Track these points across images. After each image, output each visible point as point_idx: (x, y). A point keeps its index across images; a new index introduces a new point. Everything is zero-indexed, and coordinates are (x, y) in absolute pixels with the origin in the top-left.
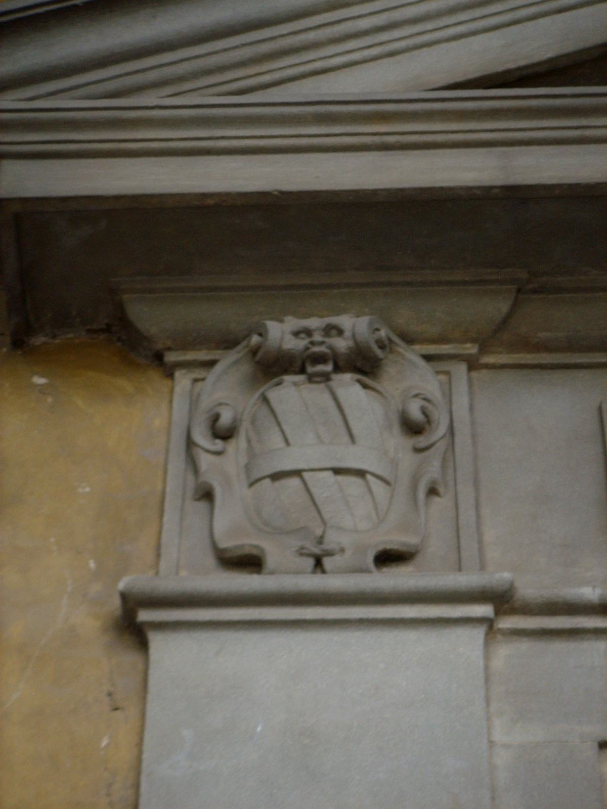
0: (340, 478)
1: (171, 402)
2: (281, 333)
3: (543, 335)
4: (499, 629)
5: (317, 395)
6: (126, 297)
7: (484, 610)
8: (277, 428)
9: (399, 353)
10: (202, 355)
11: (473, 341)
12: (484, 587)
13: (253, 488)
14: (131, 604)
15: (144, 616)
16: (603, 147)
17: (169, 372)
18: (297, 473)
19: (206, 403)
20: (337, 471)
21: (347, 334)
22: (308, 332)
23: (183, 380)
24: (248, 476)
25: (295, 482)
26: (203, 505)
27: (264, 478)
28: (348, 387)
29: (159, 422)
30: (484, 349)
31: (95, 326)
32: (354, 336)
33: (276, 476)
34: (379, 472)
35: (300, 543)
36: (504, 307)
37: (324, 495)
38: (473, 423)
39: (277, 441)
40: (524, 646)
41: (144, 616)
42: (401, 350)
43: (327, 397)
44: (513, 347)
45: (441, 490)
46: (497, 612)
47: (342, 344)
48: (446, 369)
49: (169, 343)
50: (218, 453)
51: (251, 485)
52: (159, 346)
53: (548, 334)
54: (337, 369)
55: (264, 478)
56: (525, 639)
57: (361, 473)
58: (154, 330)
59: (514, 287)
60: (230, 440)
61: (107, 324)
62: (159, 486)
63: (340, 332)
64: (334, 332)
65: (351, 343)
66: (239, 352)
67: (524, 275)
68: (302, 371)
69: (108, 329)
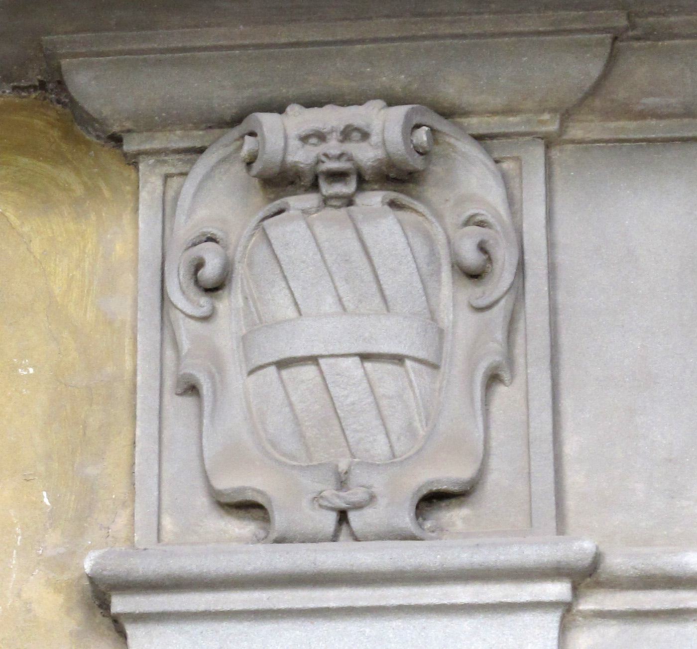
0: (368, 365)
1: (136, 210)
2: (283, 135)
3: (650, 101)
4: (580, 611)
5: (332, 228)
6: (64, 62)
7: (559, 590)
8: (283, 284)
9: (449, 144)
10: (177, 139)
11: (553, 111)
12: (559, 562)
13: (253, 377)
14: (99, 594)
15: (120, 604)
16: (693, 150)
17: (133, 160)
18: (314, 359)
19: (185, 227)
20: (365, 357)
21: (375, 139)
22: (321, 137)
23: (151, 183)
24: (247, 359)
25: (309, 371)
26: (188, 402)
27: (269, 364)
28: (380, 223)
29: (120, 249)
30: (567, 115)
31: (23, 83)
32: (384, 143)
33: (282, 364)
34: (421, 355)
35: (319, 487)
36: (595, 69)
37: (349, 401)
38: (551, 245)
39: (283, 308)
40: (612, 631)
41: (120, 604)
42: (452, 141)
43: (350, 233)
44: (608, 114)
45: (506, 376)
46: (575, 589)
47: (367, 155)
48: (515, 154)
49: (128, 125)
50: (205, 319)
51: (251, 372)
52: (116, 129)
53: (657, 100)
54: (363, 182)
55: (269, 364)
56: (613, 622)
57: (398, 359)
58: (106, 111)
59: (607, 37)
60: (220, 292)
61: (41, 82)
62: (128, 365)
63: (365, 135)
64: (356, 135)
65: (379, 154)
66: (226, 146)
67: (623, 22)
68: (314, 187)
69: (42, 85)
